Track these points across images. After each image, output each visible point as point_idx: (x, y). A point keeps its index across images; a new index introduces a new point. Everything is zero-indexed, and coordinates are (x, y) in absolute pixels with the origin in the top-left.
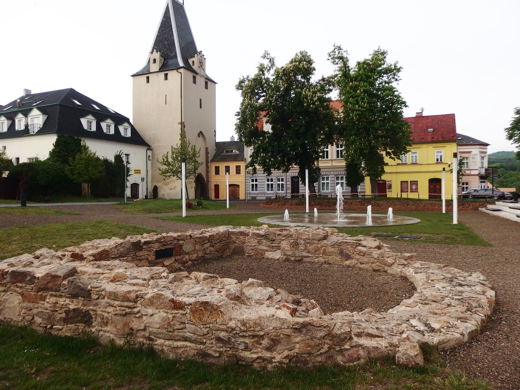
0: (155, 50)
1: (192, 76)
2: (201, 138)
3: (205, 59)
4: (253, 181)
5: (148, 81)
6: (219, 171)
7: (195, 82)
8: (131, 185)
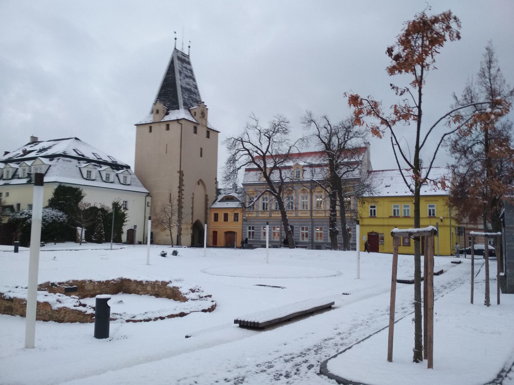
0: (158, 102)
2: (201, 186)
4: (250, 228)
5: (151, 131)
7: (195, 132)
8: (128, 231)
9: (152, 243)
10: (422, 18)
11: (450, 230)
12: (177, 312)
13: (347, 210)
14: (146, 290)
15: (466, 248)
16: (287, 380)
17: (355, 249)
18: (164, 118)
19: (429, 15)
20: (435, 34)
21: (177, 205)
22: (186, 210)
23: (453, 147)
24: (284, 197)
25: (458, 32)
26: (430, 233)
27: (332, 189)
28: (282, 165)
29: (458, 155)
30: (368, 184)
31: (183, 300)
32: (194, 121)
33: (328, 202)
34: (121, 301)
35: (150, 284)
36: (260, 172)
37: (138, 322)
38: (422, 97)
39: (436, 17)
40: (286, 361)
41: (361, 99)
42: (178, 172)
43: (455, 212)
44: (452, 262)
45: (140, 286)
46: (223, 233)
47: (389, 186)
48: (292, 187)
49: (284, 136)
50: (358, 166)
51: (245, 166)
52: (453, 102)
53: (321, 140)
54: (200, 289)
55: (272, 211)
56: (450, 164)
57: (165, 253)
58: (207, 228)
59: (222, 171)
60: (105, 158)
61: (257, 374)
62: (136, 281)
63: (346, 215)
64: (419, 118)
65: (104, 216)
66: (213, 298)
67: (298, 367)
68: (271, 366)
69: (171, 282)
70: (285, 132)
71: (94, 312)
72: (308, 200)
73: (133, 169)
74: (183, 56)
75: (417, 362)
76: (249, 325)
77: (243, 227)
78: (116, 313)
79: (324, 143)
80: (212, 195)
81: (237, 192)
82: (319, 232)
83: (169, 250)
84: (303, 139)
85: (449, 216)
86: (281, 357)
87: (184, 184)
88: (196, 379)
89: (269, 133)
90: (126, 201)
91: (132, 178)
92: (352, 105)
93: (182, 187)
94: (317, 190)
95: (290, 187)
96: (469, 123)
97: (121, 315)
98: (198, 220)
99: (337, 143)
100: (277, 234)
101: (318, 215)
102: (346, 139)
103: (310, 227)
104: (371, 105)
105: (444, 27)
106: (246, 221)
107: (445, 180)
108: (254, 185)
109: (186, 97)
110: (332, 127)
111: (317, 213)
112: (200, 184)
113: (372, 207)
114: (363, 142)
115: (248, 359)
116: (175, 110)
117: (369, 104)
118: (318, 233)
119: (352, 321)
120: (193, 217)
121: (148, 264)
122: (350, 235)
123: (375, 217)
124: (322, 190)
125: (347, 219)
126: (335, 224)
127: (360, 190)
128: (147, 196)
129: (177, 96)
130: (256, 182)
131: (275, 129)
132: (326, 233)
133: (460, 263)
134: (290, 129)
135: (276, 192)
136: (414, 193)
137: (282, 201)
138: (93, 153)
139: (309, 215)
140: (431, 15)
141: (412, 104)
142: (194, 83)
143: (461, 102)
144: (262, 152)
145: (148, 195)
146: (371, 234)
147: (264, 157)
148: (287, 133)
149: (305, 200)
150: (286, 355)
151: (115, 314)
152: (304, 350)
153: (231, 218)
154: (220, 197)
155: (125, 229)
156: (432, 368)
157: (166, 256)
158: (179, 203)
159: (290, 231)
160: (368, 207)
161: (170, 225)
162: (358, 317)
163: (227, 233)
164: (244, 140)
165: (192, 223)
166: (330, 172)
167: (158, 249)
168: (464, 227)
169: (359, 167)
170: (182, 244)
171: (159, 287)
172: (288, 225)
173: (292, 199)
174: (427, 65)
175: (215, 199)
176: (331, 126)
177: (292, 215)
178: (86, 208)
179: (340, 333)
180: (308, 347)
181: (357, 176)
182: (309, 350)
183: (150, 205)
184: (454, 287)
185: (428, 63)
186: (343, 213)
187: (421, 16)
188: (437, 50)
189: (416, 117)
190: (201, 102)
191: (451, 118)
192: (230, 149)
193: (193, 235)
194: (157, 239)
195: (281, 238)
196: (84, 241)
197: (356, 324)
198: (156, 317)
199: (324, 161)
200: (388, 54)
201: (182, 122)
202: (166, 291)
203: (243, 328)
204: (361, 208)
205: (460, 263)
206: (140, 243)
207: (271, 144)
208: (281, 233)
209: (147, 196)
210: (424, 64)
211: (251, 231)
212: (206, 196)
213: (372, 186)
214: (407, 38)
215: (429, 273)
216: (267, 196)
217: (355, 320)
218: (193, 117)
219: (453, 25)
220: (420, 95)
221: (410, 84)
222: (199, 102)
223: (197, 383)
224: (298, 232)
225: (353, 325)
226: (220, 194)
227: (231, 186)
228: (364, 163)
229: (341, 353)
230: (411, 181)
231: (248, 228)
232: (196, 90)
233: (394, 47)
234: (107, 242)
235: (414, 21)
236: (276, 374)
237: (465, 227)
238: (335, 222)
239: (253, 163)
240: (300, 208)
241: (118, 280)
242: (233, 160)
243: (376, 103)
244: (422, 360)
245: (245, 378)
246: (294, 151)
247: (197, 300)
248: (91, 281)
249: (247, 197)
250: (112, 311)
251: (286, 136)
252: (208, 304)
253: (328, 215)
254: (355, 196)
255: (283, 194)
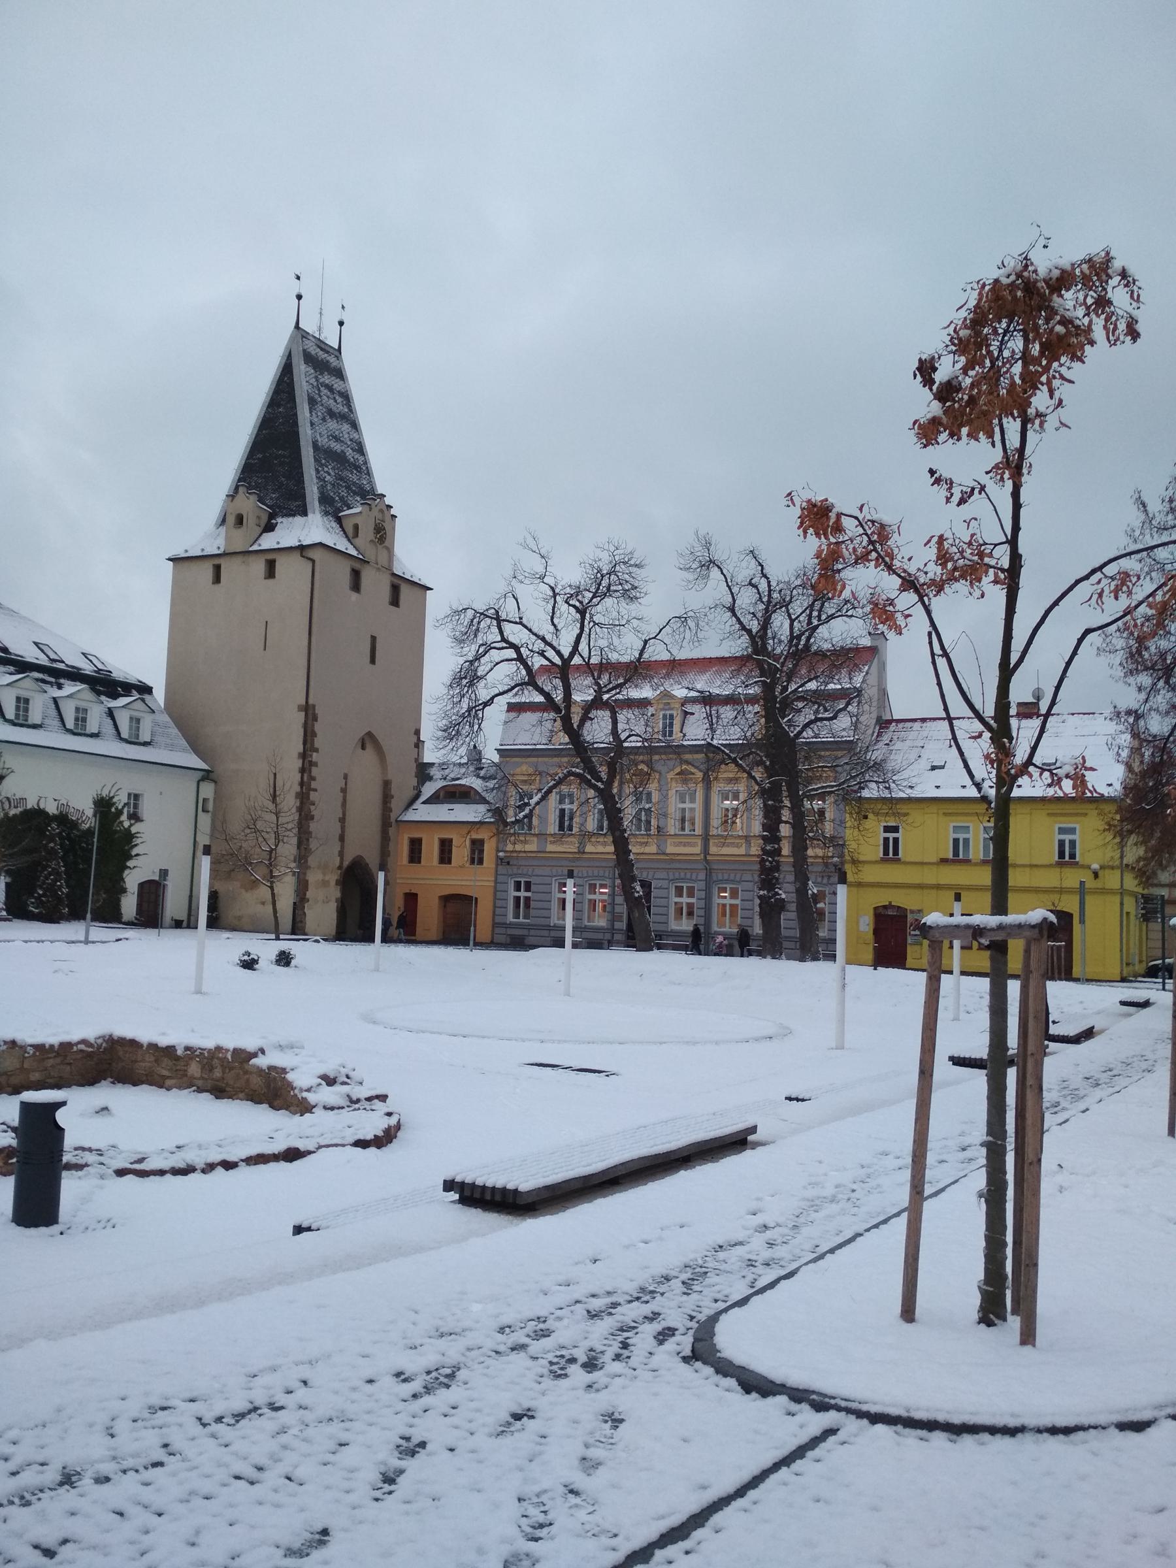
0: (241, 489)
1: (348, 570)
2: (369, 754)
3: (394, 517)
4: (518, 887)
5: (217, 579)
6: (450, 851)
7: (356, 586)
9: (214, 923)
10: (1022, 271)
11: (1122, 904)
12: (278, 1147)
13: (812, 839)
14: (186, 1075)
15: (1167, 961)
16: (586, 1378)
17: (832, 957)
18: (259, 541)
19: (1044, 264)
20: (1059, 323)
21: (294, 810)
22: (324, 824)
23: (1132, 655)
24: (624, 795)
25: (1132, 318)
26: (1037, 930)
27: (770, 771)
28: (620, 697)
29: (1145, 679)
30: (878, 761)
31: (298, 1109)
32: (354, 552)
33: (757, 812)
34: (105, 1109)
35: (197, 1056)
36: (552, 715)
37: (152, 1177)
38: (1023, 512)
39: (1063, 271)
40: (593, 1315)
41: (839, 515)
42: (300, 708)
43: (1134, 852)
44: (1123, 1003)
45: (166, 1062)
46: (437, 901)
47: (942, 767)
48: (649, 764)
49: (626, 609)
50: (848, 704)
51: (505, 696)
52: (1135, 517)
53: (739, 621)
54: (351, 1074)
55: (585, 836)
56: (1123, 706)
57: (251, 957)
58: (387, 883)
59: (434, 708)
60: (73, 659)
61: (497, 1356)
62: (153, 1047)
63: (810, 852)
64: (1012, 578)
65: (69, 838)
66: (389, 1105)
67: (626, 1334)
68: (545, 1333)
69: (263, 1051)
70: (630, 594)
71: (14, 1143)
72: (698, 805)
73: (159, 695)
74: (322, 349)
75: (990, 1324)
76: (488, 1197)
77: (496, 882)
78: (87, 1145)
79: (749, 632)
80: (404, 782)
81: (482, 773)
82: (728, 902)
83: (265, 948)
84: (683, 619)
85: (1117, 863)
86: (577, 1302)
87: (316, 746)
88: (306, 1373)
89: (580, 597)
90: (137, 792)
91: (156, 724)
92: (811, 531)
93: (311, 756)
94: (725, 775)
95: (642, 762)
96: (1159, 597)
97: (100, 1152)
98: (361, 857)
99: (788, 633)
100: (599, 906)
101: (726, 850)
102: (815, 622)
103: (702, 885)
104: (869, 532)
105: (1090, 301)
106: (508, 863)
107: (1087, 769)
108: (534, 753)
109: (328, 478)
110: (774, 584)
111: (724, 845)
112: (368, 746)
113: (887, 829)
114: (865, 633)
115: (476, 1308)
116: (294, 516)
117: (862, 531)
118: (724, 906)
119: (805, 1188)
120: (342, 847)
121: (199, 992)
122: (821, 913)
123: (896, 860)
124: (739, 775)
125: (812, 864)
126: (777, 879)
127: (852, 777)
128: (203, 779)
129: (301, 475)
130: (538, 747)
131: (600, 584)
132: (748, 905)
133: (1146, 1004)
134: (644, 587)
135: (599, 779)
136: (993, 805)
137: (618, 806)
138: (36, 644)
139: (697, 850)
140: (1049, 264)
141: (992, 532)
142: (356, 436)
143: (1159, 519)
144: (559, 653)
145: (207, 776)
146: (882, 911)
147: (564, 670)
148: (637, 598)
149: (687, 805)
150: (593, 1296)
151: (83, 1149)
152: (651, 1281)
153: (461, 853)
154: (429, 790)
155: (132, 880)
156: (1034, 1345)
157: (256, 966)
158: (302, 803)
159: (640, 897)
160: (875, 828)
161: (271, 871)
162: (826, 1175)
163: (447, 899)
164: (503, 616)
165: (340, 868)
166: (763, 720)
167: (233, 945)
168: (1163, 896)
169: (850, 708)
170: (307, 930)
171: (226, 1066)
172: (633, 879)
173: (649, 800)
174: (1039, 415)
175: (412, 793)
176: (769, 582)
177: (647, 850)
178: (12, 812)
179: (765, 1226)
180: (664, 1272)
181: (844, 733)
182: (667, 1279)
183: (210, 806)
184: (1121, 1082)
185: (1042, 409)
186: (799, 847)
187: (1019, 267)
188: (1063, 370)
189: (1002, 576)
190: (375, 495)
191: (1105, 582)
192: (460, 641)
193: (342, 902)
194: (230, 912)
195: (614, 918)
196: (4, 913)
197: (819, 1198)
198: (210, 1160)
199: (747, 686)
200: (919, 378)
201: (316, 555)
202: (248, 1080)
203: (470, 1206)
204: (856, 832)
205: (1146, 1004)
206: (178, 924)
207: (586, 629)
208: (613, 904)
209: (203, 779)
210: (1031, 411)
211: (523, 894)
212: (387, 784)
213: (889, 766)
214: (978, 334)
215: (1029, 1053)
216: (572, 788)
217: (814, 1184)
218: (349, 540)
219: (1119, 296)
220: (1017, 506)
221: (987, 473)
222: (368, 494)
223: (310, 1384)
224: (663, 902)
225: (808, 1200)
226: (430, 778)
227: (461, 757)
228: (866, 695)
229: (762, 1291)
230: (981, 770)
231: (512, 886)
232: (361, 459)
233: (939, 358)
234: (75, 920)
235: (997, 281)
236: (557, 1356)
237: (1166, 897)
238: (776, 874)
239: (531, 688)
240: (672, 827)
241: (100, 1041)
242: (468, 677)
243: (883, 526)
244: (1005, 1319)
245: (459, 1369)
246: (658, 652)
247: (343, 1108)
248: (13, 1043)
249: (512, 792)
250: (69, 1142)
251: (633, 606)
252: (372, 1123)
253: (755, 850)
254: (838, 795)
255: (621, 784)
